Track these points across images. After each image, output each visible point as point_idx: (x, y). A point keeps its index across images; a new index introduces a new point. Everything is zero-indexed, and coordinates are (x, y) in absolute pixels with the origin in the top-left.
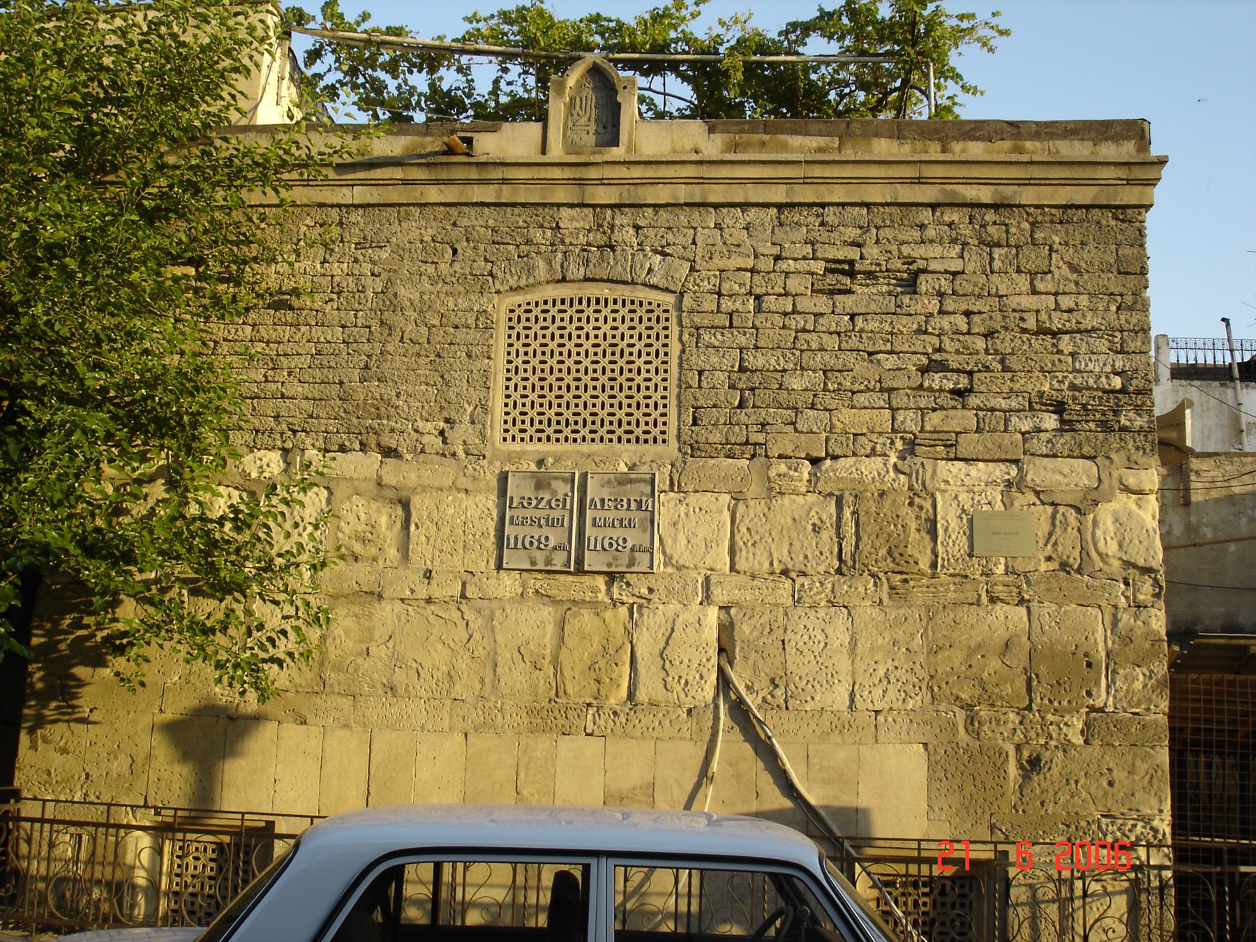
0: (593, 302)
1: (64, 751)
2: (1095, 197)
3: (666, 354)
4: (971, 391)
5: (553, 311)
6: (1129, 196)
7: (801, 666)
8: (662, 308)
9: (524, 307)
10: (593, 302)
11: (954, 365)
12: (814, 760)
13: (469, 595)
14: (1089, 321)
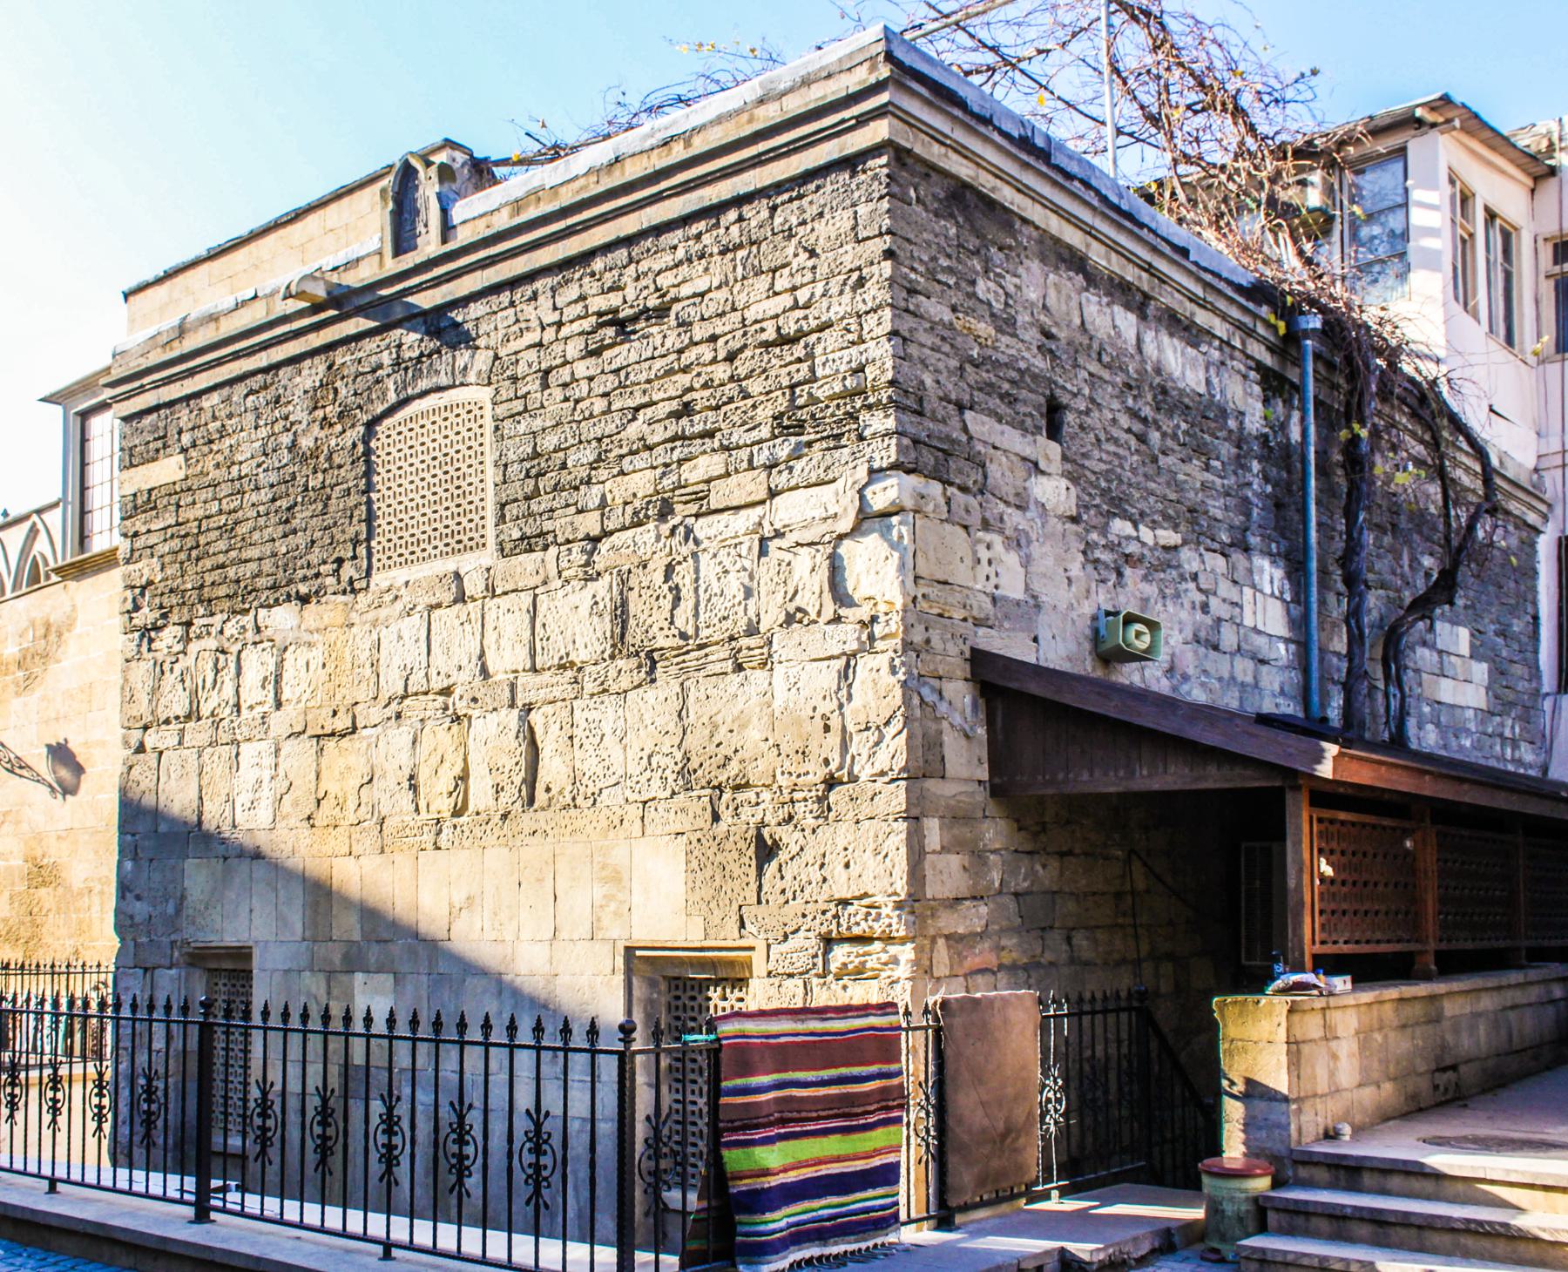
1: (138, 898)
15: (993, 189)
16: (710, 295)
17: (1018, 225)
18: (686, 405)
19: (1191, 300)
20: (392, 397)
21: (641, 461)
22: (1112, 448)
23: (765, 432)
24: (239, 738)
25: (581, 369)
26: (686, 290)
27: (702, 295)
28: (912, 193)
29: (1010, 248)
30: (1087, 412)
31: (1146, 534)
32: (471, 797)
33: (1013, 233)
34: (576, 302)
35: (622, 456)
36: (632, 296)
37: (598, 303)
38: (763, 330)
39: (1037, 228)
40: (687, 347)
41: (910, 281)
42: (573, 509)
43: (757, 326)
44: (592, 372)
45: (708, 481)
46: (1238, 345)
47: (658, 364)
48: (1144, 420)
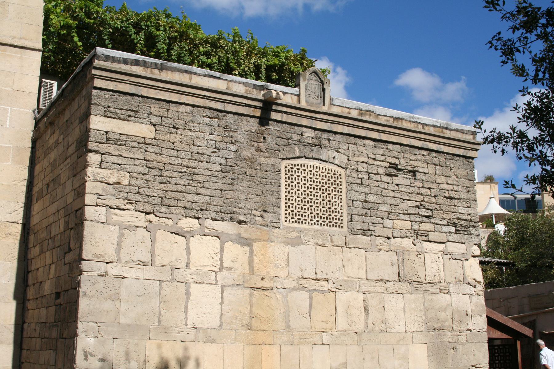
0: (303, 166)
2: (463, 153)
3: (341, 206)
4: (432, 216)
5: (301, 169)
6: (471, 154)
7: (390, 316)
8: (339, 174)
9: (290, 166)
10: (303, 166)
11: (427, 207)
12: (396, 351)
13: (350, 159)
14: (462, 196)
20: (297, 154)
21: (406, 217)
23: (445, 222)
24: (191, 281)
35: (400, 214)
42: (382, 226)
45: (428, 231)
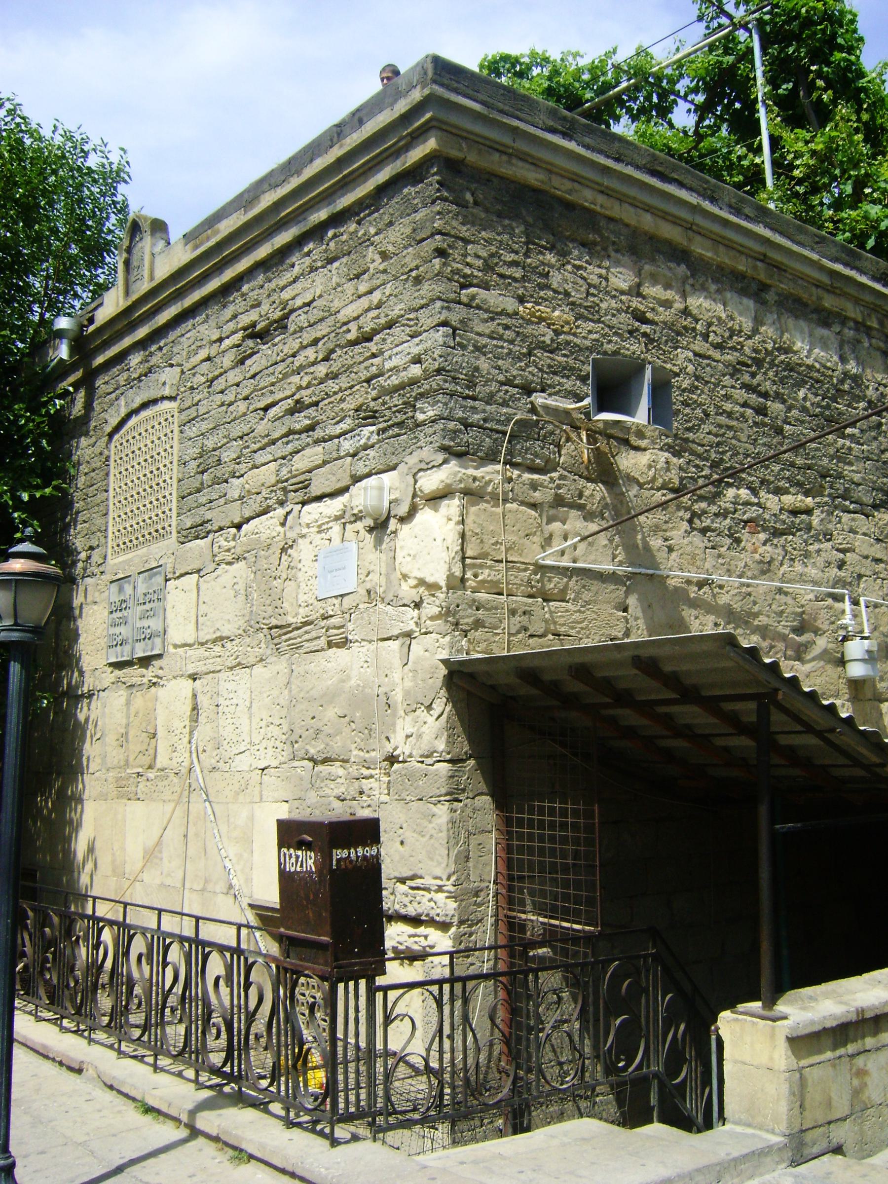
15: (569, 192)
16: (314, 304)
17: (603, 223)
18: (298, 402)
19: (817, 286)
22: (722, 419)
25: (233, 376)
26: (299, 302)
27: (308, 304)
28: (468, 196)
29: (595, 244)
30: (693, 389)
31: (772, 502)
32: (159, 756)
33: (597, 230)
34: (231, 320)
36: (269, 311)
37: (245, 320)
38: (349, 331)
39: (627, 226)
40: (298, 352)
41: (465, 276)
43: (345, 328)
44: (237, 380)
46: (875, 325)
47: (280, 367)
48: (765, 395)
